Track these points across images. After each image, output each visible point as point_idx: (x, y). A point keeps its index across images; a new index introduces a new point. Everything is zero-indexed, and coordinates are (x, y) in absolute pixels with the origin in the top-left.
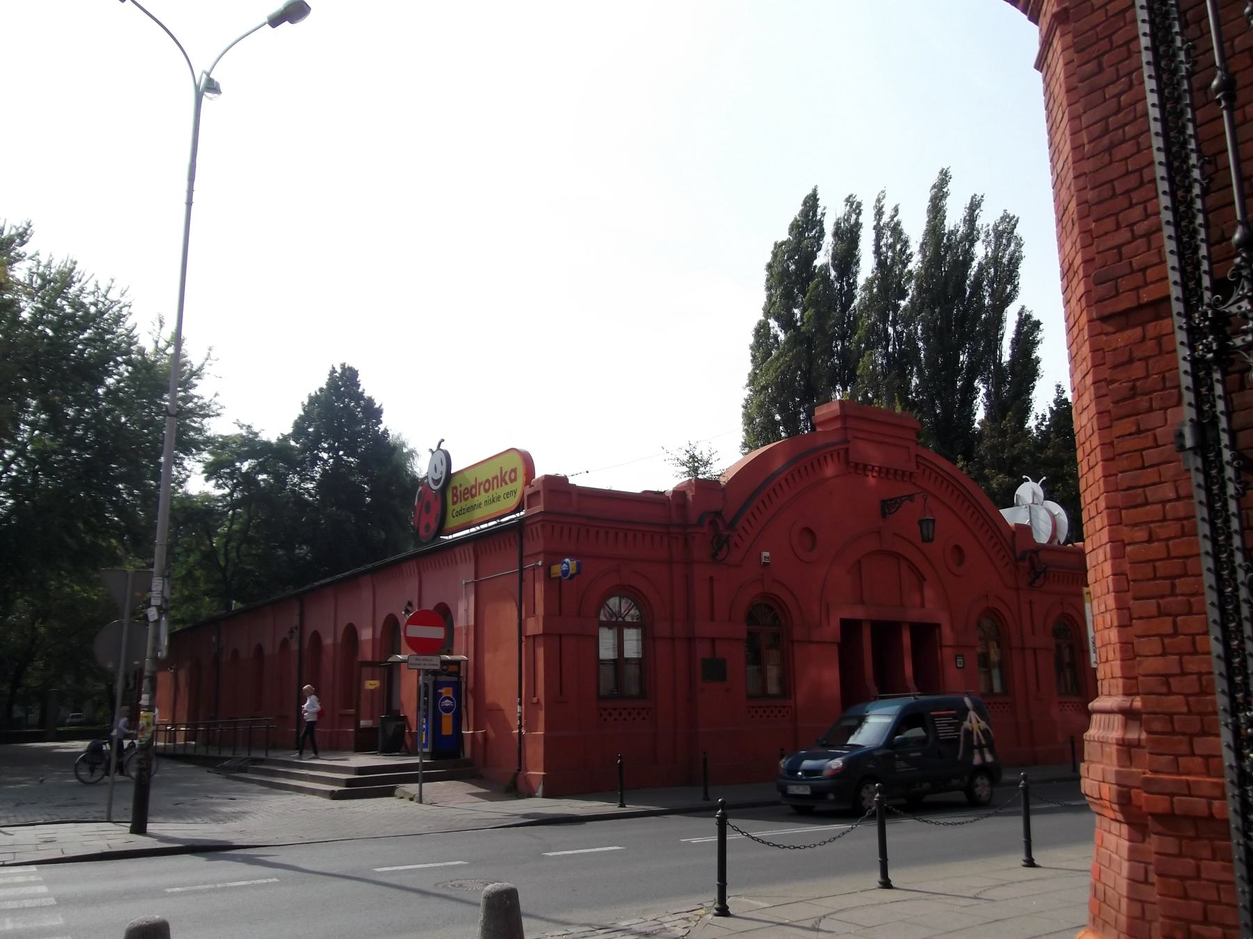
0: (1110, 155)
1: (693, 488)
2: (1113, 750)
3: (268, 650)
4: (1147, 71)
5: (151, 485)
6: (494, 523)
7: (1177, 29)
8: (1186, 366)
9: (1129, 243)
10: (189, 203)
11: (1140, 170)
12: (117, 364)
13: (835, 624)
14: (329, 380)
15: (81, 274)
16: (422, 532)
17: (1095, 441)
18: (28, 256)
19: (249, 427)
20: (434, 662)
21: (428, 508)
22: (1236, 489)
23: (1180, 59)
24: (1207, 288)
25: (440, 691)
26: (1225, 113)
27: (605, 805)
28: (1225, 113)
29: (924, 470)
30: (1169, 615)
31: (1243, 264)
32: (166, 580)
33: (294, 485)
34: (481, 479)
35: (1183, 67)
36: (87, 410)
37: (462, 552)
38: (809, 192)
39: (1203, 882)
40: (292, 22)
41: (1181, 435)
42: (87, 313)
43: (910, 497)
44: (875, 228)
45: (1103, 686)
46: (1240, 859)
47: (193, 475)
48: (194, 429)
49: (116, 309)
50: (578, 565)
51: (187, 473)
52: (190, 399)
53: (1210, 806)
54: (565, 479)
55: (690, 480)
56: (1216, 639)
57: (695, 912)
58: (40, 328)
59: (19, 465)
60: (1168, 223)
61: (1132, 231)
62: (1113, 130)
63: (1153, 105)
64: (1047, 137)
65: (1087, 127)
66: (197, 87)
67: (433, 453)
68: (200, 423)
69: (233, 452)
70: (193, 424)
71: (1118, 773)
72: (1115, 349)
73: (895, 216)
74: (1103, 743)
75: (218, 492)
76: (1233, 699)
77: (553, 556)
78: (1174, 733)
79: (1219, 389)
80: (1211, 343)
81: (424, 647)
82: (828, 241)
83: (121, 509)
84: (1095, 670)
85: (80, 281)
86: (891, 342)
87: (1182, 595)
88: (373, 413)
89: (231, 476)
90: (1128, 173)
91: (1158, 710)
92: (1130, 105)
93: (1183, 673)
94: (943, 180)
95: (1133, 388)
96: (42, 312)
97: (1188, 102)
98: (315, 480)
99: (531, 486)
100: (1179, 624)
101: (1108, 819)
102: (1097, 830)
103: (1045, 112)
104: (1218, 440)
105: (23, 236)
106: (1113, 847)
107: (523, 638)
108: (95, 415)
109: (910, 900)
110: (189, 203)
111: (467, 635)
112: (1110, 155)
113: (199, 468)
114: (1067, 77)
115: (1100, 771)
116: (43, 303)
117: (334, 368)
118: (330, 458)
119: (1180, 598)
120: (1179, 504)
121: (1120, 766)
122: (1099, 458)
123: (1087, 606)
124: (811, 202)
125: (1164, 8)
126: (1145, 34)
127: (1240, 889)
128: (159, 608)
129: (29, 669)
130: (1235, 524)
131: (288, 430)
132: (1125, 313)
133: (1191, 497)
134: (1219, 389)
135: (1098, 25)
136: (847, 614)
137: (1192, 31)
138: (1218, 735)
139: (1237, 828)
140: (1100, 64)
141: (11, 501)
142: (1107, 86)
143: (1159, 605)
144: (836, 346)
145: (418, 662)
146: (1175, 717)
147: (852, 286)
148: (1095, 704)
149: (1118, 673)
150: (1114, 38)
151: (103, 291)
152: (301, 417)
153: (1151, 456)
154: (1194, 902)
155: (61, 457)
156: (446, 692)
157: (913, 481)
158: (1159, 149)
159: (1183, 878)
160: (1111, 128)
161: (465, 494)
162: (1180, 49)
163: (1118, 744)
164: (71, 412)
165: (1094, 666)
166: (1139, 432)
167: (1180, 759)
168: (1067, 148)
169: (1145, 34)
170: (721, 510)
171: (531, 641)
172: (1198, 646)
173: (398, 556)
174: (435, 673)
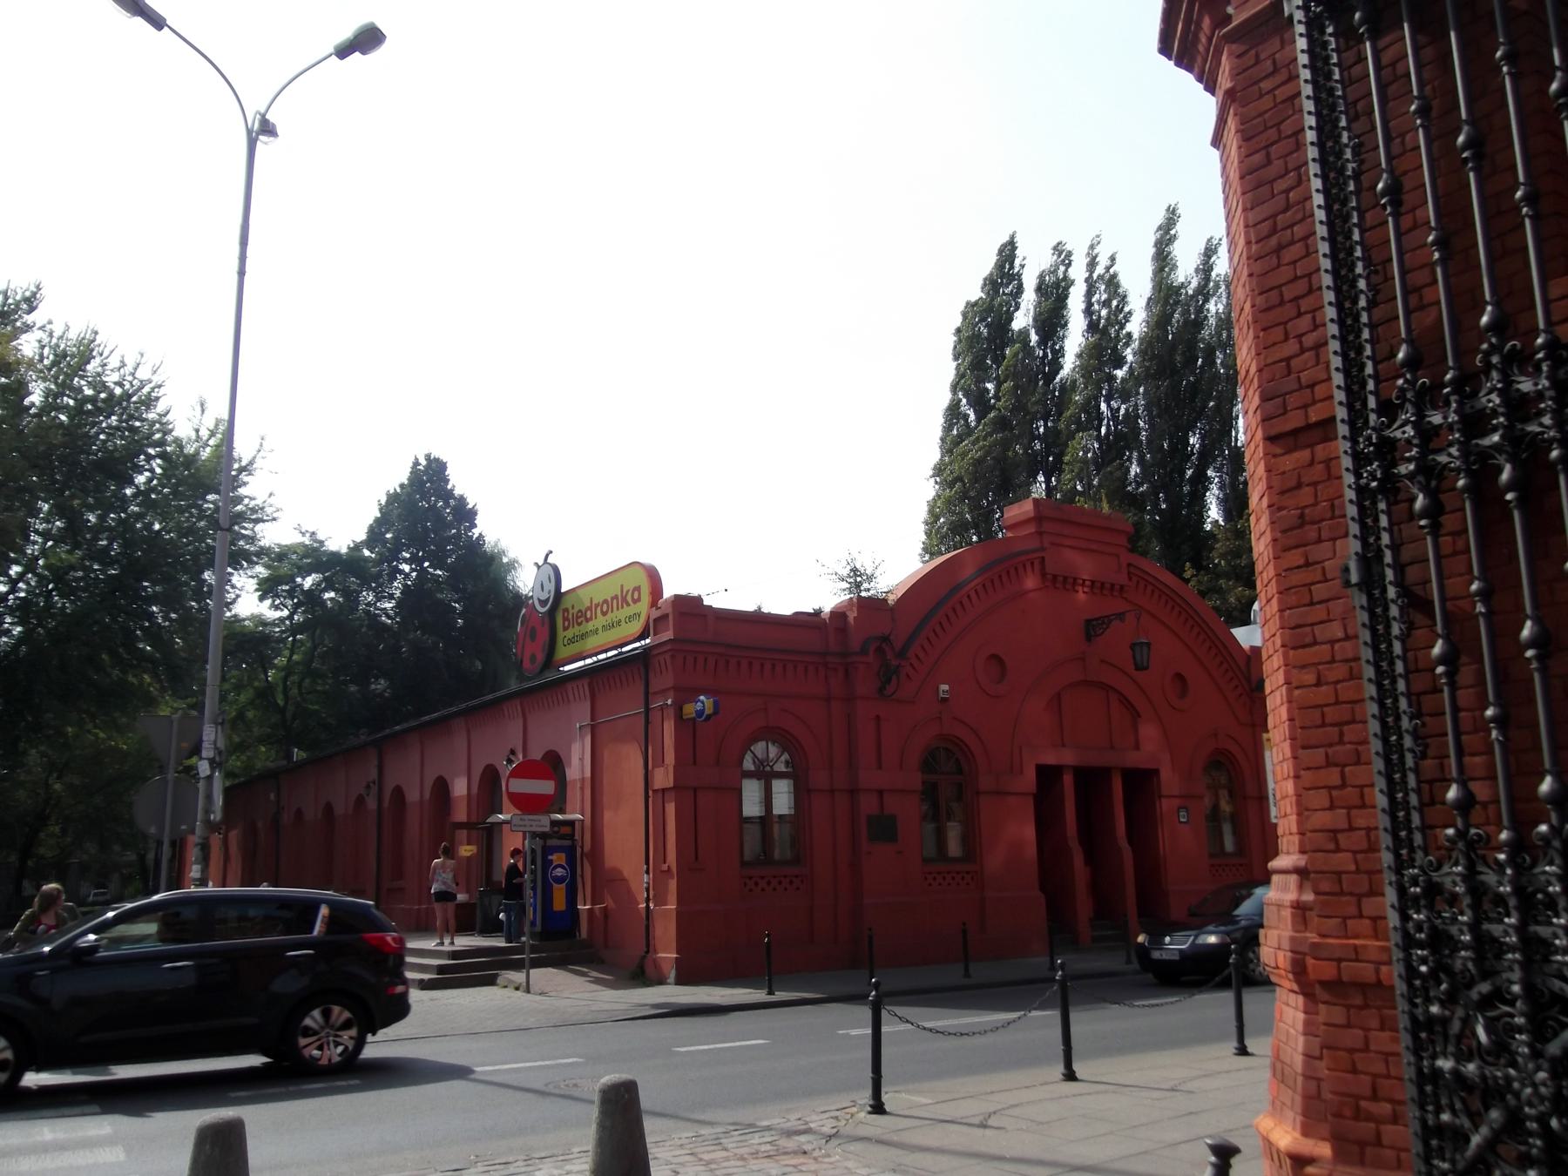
0: (1278, 258)
1: (855, 609)
2: (1287, 913)
3: (339, 810)
4: (1314, 168)
5: (192, 607)
6: (615, 652)
7: (1343, 123)
8: (1350, 494)
9: (1297, 355)
10: (242, 273)
11: (1309, 275)
12: (149, 458)
13: (1030, 775)
14: (411, 473)
15: (102, 346)
16: (527, 664)
17: (1271, 571)
18: (38, 326)
19: (313, 533)
20: (542, 822)
21: (532, 633)
22: (1401, 629)
23: (1345, 157)
24: (1372, 410)
25: (550, 857)
26: (1390, 219)
27: (751, 993)
28: (1390, 219)
29: (1138, 582)
30: (1336, 765)
31: (1406, 386)
32: (219, 727)
33: (369, 604)
34: (598, 599)
35: (1350, 166)
36: (112, 515)
37: (580, 687)
38: (1006, 239)
39: (1372, 1055)
40: (364, 53)
41: (1347, 570)
42: (111, 394)
43: (1120, 616)
44: (1087, 280)
45: (1283, 843)
46: (1405, 1029)
47: (243, 594)
48: (244, 536)
49: (146, 390)
50: (716, 704)
51: (238, 592)
52: (239, 500)
53: (1377, 972)
54: (699, 599)
55: (851, 598)
56: (1381, 791)
57: (847, 1110)
58: (53, 414)
59: (28, 584)
60: (1334, 337)
61: (1301, 343)
62: (1282, 230)
63: (1319, 207)
64: (1224, 224)
65: (1255, 225)
66: (249, 132)
67: (539, 567)
68: (252, 530)
69: (294, 565)
70: (243, 531)
71: (1292, 939)
72: (1284, 473)
73: (1111, 266)
74: (1279, 906)
75: (274, 615)
76: (1397, 856)
77: (686, 693)
78: (1342, 893)
79: (1384, 521)
80: (1375, 471)
81: (528, 804)
82: (1029, 298)
83: (154, 634)
84: (1276, 825)
85: (101, 355)
86: (1105, 422)
87: (1350, 743)
88: (466, 515)
89: (291, 594)
90: (1296, 278)
91: (1325, 868)
92: (1299, 203)
93: (1351, 829)
94: (1169, 219)
95: (1302, 516)
96: (56, 396)
97: (1354, 204)
98: (394, 599)
99: (658, 608)
100: (1347, 774)
101: (1286, 991)
102: (1278, 1003)
103: (1222, 196)
104: (1383, 576)
105: (31, 302)
106: (1290, 1021)
107: (651, 793)
108: (120, 521)
109: (1097, 1093)
110: (242, 273)
111: (582, 789)
112: (1278, 258)
113: (252, 584)
114: (1241, 162)
115: (1276, 938)
116: (56, 383)
117: (416, 459)
118: (412, 570)
119: (1348, 746)
120: (1347, 644)
121: (1297, 931)
122: (1275, 591)
123: (1267, 754)
124: (1008, 252)
125: (1331, 100)
126: (1311, 128)
127: (1405, 1061)
128: (212, 762)
129: (42, 835)
130: (1399, 667)
131: (361, 535)
132: (1295, 432)
133: (1356, 637)
134: (1384, 521)
135: (1266, 112)
136: (1050, 759)
137: (1358, 127)
138: (1383, 895)
139: (1402, 995)
140: (1268, 154)
141: (19, 629)
142: (1275, 180)
143: (1327, 755)
144: (1038, 428)
145: (521, 823)
146: (1344, 876)
147: (1058, 354)
148: (1275, 864)
149: (1294, 829)
150: (1282, 127)
151: (129, 369)
152: (377, 520)
153: (1320, 591)
154: (1362, 1076)
155: (80, 574)
156: (558, 858)
157: (1125, 595)
158: (1325, 255)
159: (1351, 1051)
160: (1279, 227)
161: (578, 618)
162: (1347, 146)
163: (1292, 907)
164: (92, 518)
165: (1274, 821)
166: (1307, 564)
167: (1349, 922)
168: (1241, 242)
169: (1311, 128)
170: (889, 635)
171: (660, 795)
172: (1366, 798)
173: (498, 694)
174: (543, 836)
